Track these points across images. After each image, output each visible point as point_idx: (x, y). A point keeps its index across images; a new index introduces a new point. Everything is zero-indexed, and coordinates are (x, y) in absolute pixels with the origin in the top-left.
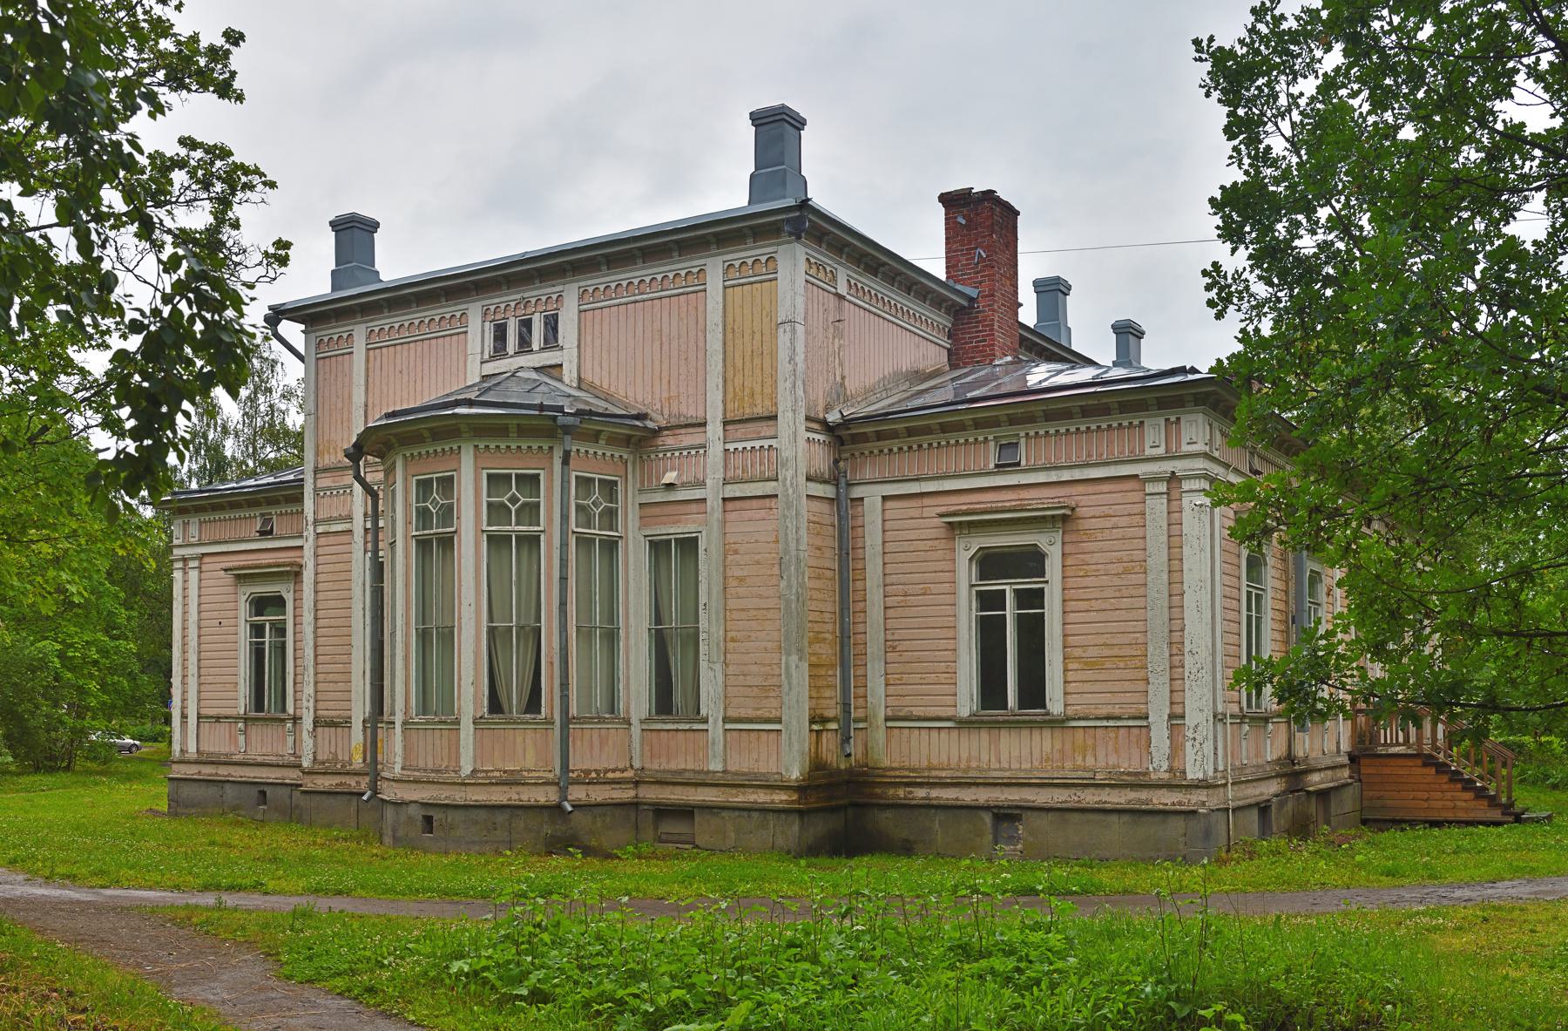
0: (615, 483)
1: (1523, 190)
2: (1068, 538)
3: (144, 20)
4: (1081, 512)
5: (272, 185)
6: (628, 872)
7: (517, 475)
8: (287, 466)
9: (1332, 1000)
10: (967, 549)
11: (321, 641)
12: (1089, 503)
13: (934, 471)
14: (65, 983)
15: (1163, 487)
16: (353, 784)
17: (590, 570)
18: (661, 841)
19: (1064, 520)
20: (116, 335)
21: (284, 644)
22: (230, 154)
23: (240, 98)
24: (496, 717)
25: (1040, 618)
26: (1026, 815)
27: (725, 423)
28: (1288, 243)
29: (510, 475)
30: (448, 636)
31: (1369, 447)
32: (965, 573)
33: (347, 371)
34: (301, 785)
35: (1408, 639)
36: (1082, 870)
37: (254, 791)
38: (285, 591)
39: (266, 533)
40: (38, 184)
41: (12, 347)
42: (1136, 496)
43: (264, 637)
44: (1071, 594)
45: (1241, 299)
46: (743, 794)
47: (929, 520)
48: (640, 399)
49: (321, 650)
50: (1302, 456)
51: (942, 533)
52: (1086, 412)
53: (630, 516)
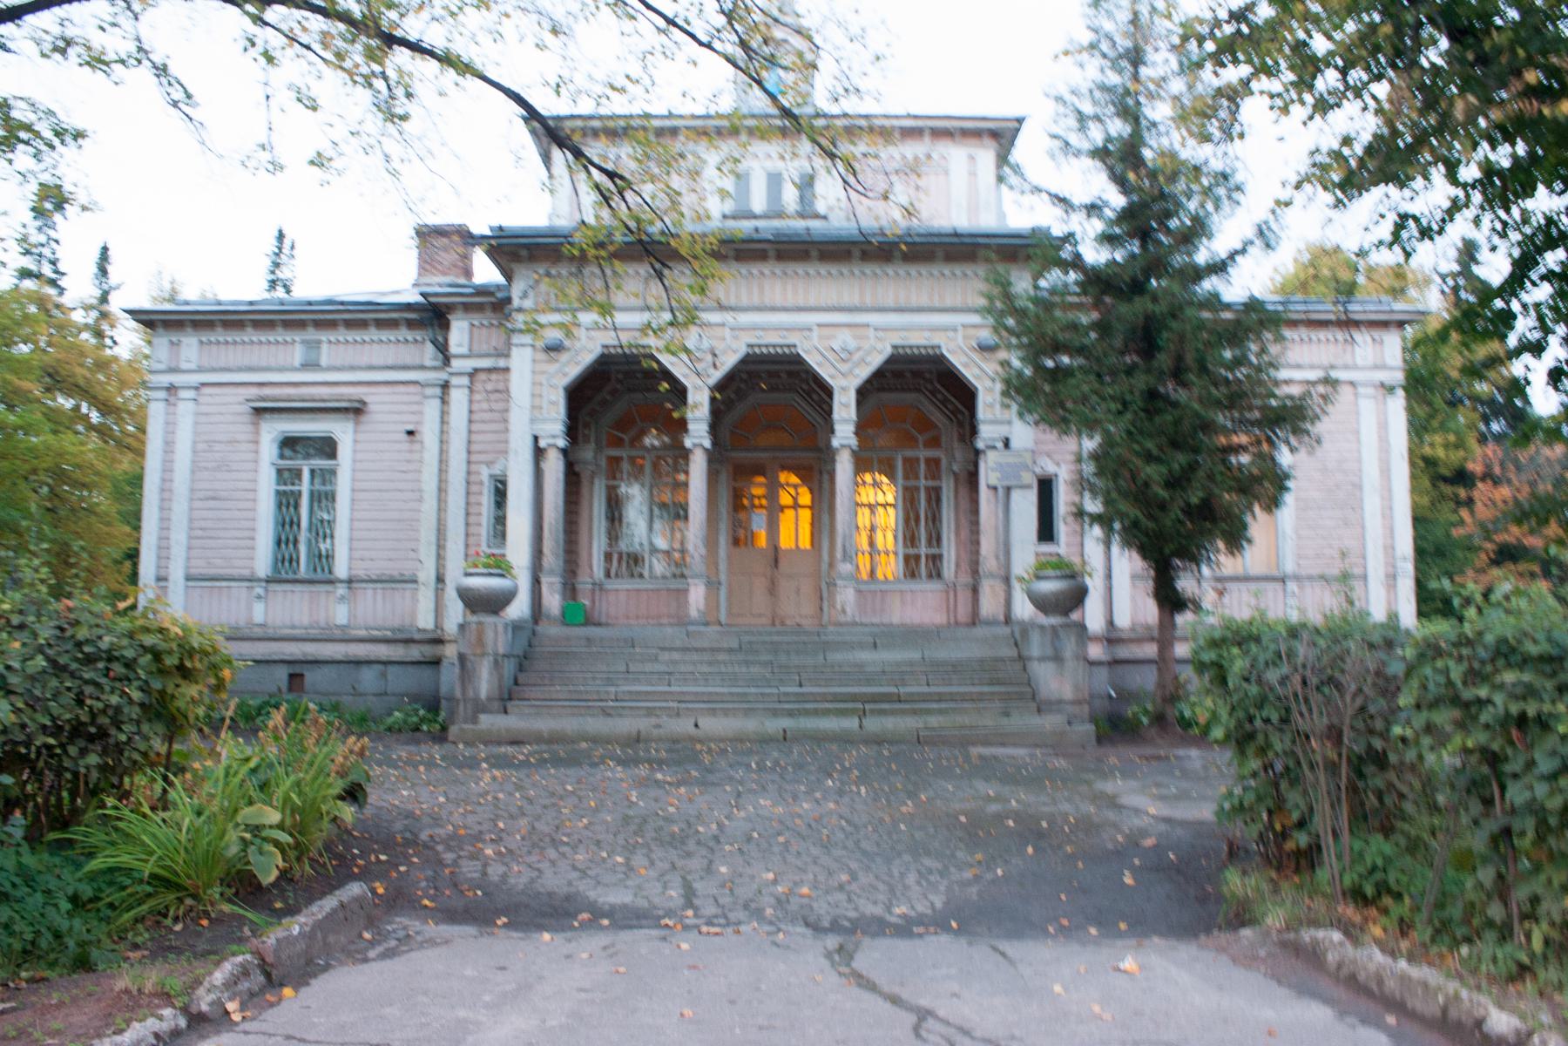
1: (1494, 362)
2: (361, 437)
4: (372, 407)
5: (79, 135)
8: (245, 887)
10: (273, 430)
12: (373, 397)
13: (790, 302)
15: (465, 381)
18: (496, 662)
19: (356, 411)
21: (464, 304)
23: (1020, 121)
24: (297, 669)
25: (940, 557)
29: (918, 460)
31: (1534, 616)
32: (268, 450)
33: (622, 123)
35: (15, 306)
37: (282, 674)
38: (341, 431)
39: (310, 365)
42: (417, 398)
43: (917, 478)
44: (357, 534)
45: (283, 891)
46: (757, 230)
47: (235, 403)
49: (474, 447)
50: (1410, 653)
51: (247, 418)
52: (350, 324)
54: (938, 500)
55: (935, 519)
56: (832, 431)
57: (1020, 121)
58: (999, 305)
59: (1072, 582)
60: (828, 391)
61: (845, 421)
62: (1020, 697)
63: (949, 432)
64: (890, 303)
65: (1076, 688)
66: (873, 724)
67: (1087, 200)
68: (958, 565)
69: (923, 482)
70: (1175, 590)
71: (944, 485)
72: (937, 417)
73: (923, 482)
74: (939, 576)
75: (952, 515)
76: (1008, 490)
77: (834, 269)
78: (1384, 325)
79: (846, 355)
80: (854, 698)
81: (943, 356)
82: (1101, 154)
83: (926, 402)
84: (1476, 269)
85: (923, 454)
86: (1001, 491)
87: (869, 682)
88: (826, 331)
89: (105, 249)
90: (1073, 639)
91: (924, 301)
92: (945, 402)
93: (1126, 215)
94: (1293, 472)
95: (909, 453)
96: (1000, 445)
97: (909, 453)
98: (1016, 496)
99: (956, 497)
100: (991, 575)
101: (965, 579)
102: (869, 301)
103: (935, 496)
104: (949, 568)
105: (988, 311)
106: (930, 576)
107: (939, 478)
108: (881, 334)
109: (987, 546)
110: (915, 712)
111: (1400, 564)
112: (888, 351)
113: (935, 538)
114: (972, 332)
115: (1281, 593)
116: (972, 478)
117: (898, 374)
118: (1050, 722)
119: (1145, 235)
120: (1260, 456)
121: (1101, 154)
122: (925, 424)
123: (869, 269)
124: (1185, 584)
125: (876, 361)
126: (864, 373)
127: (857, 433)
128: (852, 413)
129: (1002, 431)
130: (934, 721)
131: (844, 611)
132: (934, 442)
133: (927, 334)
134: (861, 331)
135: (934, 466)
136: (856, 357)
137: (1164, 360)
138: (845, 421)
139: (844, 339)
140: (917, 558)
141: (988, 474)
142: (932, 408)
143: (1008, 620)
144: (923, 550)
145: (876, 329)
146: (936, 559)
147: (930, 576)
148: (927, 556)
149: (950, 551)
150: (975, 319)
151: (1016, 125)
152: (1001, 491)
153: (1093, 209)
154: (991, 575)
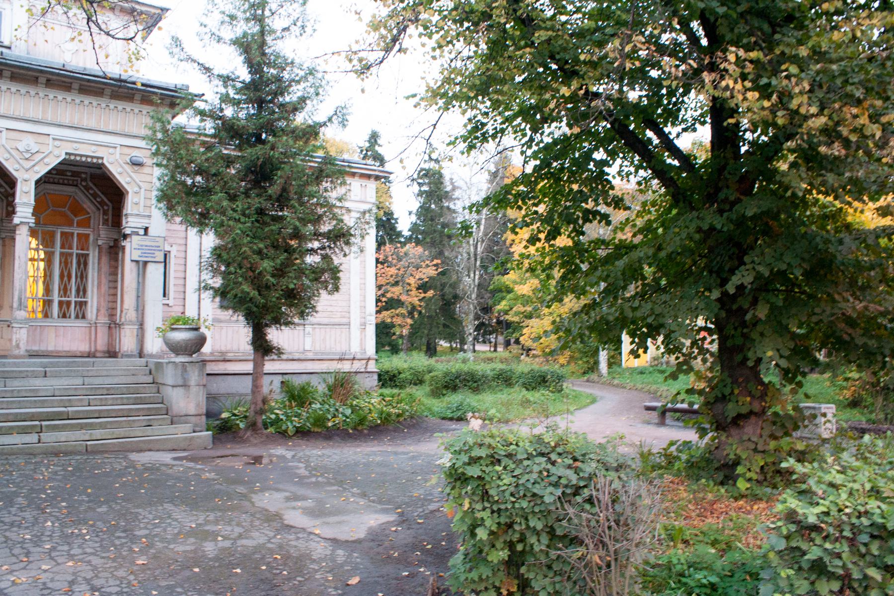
0: (89, 235)
3: (574, 213)
6: (49, 533)
7: (78, 234)
9: (232, 269)
11: (183, 242)
14: (320, 90)
16: (25, 189)
17: (9, 363)
20: (476, 49)
22: (647, 201)
26: (208, 364)
27: (349, 324)
28: (461, 102)
29: (72, 234)
30: (62, 276)
34: (288, 499)
36: (550, 394)
40: (767, 66)
41: (112, 326)
43: (71, 248)
48: (224, 331)
53: (99, 335)
54: (86, 264)
55: (82, 276)
56: (14, 212)
57: (164, 10)
58: (159, 136)
59: (195, 332)
60: (12, 183)
61: (25, 204)
62: (157, 412)
63: (97, 218)
64: (67, 122)
65: (198, 405)
66: (49, 437)
67: (225, 73)
68: (98, 310)
69: (75, 251)
70: (266, 341)
71: (91, 253)
72: (87, 205)
73: (75, 251)
74: (84, 317)
75: (96, 274)
76: (145, 263)
77: (23, 89)
78: (369, 177)
79: (28, 155)
80: (32, 417)
81: (103, 164)
82: (236, 42)
83: (80, 194)
84: (377, 148)
85: (76, 231)
86: (141, 264)
87: (43, 404)
88: (13, 135)
89: (408, 98)
90: (196, 373)
91: (93, 124)
92: (95, 196)
93: (247, 87)
94: (341, 268)
95: (67, 230)
96: (142, 232)
97: (67, 230)
98: (150, 267)
99: (99, 263)
100: (131, 323)
101: (104, 319)
102: (49, 118)
103: (83, 261)
104: (91, 311)
105: (152, 139)
106: (77, 317)
107: (88, 250)
108: (57, 143)
109: (129, 301)
110: (82, 427)
111: (368, 318)
112: (63, 157)
113: (82, 290)
114: (126, 151)
115: (302, 332)
116: (114, 251)
117: (75, 174)
118: (181, 432)
119: (260, 103)
120: (325, 257)
121: (236, 42)
122: (77, 209)
123: (52, 93)
124: (275, 335)
125: (53, 162)
126: (43, 170)
127: (33, 215)
128: (31, 199)
129: (144, 222)
130: (97, 433)
131: (18, 346)
132: (85, 224)
133: (94, 148)
134: (42, 139)
135: (84, 240)
136: (38, 157)
137: (274, 190)
138: (25, 204)
139: (28, 143)
140: (68, 303)
141: (132, 249)
142: (83, 197)
143: (141, 355)
144: (73, 299)
145: (54, 139)
146: (82, 305)
147: (77, 317)
148: (76, 302)
149: (93, 299)
150: (142, 144)
151: (159, 11)
152: (141, 264)
153: (226, 80)
154: (131, 323)
